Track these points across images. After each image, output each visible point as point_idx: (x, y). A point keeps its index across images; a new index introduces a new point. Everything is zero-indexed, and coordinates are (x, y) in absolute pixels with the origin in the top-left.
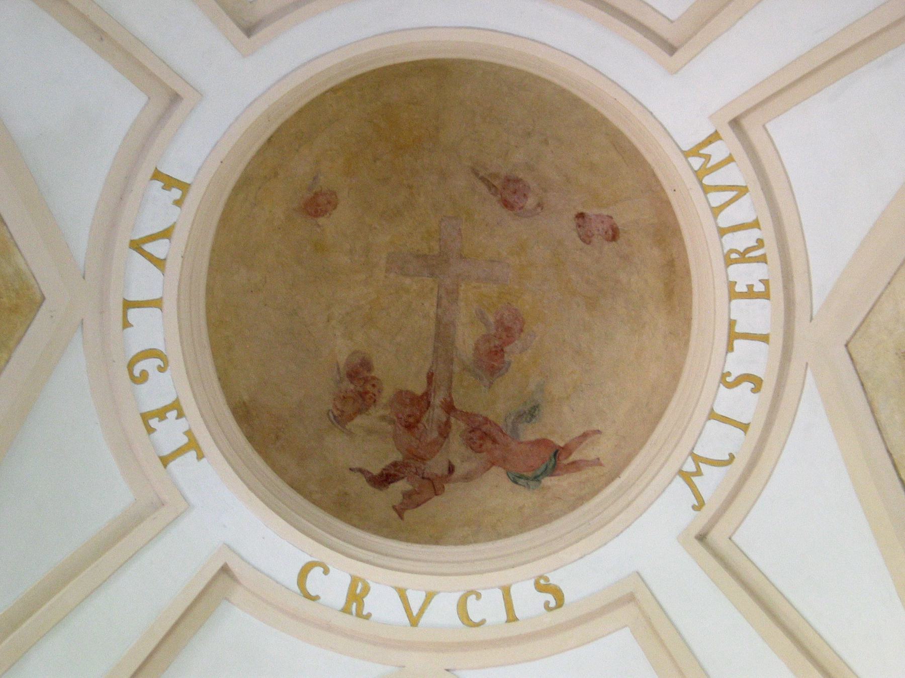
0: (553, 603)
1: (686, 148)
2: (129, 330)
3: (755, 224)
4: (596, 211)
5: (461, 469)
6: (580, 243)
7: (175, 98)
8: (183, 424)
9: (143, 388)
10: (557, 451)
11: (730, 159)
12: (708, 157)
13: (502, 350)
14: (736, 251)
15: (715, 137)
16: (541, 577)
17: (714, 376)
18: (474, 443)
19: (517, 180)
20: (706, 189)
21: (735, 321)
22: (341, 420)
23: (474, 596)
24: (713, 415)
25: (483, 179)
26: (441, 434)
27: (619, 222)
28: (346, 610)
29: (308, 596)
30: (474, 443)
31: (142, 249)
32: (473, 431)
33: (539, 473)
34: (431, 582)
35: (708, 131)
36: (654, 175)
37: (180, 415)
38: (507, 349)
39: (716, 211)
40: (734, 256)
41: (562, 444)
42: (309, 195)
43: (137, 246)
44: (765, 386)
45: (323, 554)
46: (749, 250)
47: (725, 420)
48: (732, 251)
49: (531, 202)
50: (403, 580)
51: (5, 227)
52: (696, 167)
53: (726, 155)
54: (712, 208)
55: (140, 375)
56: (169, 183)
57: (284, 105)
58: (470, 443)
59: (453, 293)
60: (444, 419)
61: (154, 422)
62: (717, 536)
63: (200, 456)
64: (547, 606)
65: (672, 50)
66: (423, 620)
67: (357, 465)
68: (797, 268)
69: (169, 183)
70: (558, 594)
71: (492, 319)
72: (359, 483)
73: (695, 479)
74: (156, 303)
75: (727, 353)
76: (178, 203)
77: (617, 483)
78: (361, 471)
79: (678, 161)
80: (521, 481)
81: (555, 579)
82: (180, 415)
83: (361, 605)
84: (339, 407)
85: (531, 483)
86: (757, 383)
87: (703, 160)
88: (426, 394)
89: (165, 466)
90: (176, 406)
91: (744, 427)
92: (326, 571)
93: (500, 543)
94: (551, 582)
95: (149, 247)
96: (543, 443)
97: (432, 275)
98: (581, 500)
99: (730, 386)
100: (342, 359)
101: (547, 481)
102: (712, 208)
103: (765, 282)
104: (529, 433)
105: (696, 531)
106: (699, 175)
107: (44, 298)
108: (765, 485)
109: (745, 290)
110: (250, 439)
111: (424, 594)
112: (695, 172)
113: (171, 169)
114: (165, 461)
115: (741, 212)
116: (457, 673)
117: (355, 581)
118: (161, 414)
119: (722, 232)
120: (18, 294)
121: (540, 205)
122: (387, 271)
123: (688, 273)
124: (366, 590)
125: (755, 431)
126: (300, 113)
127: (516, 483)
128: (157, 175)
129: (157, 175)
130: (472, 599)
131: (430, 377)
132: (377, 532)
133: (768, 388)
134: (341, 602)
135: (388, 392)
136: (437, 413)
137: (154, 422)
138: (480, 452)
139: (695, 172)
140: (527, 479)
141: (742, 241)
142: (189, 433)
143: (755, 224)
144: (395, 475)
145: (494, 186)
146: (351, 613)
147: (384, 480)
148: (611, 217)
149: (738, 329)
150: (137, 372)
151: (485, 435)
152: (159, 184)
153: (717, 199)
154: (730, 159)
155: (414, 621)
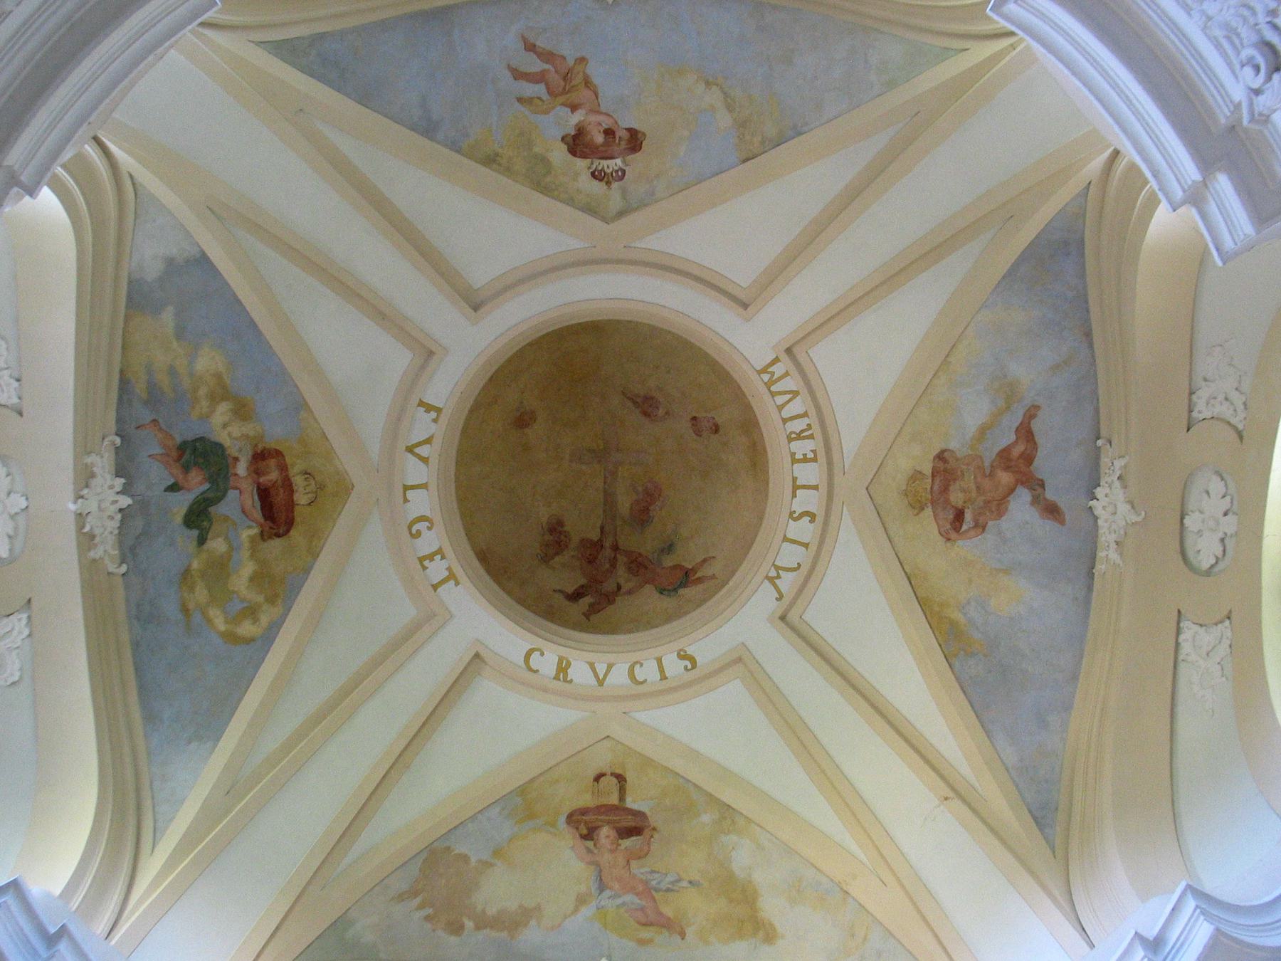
0: (689, 667)
1: (758, 368)
3: (805, 415)
4: (704, 415)
5: (626, 586)
6: (695, 437)
7: (431, 353)
8: (444, 564)
9: (418, 541)
10: (686, 573)
11: (787, 374)
12: (773, 374)
13: (648, 509)
14: (794, 433)
15: (776, 361)
16: (681, 650)
17: (785, 515)
18: (633, 570)
19: (652, 398)
20: (773, 394)
21: (797, 478)
22: (546, 559)
23: (638, 666)
24: (785, 539)
25: (629, 398)
26: (611, 566)
27: (719, 420)
28: (556, 678)
29: (531, 670)
30: (633, 570)
32: (632, 562)
33: (676, 586)
34: (611, 658)
35: (772, 357)
36: (740, 388)
37: (443, 558)
38: (652, 508)
39: (780, 408)
40: (793, 436)
41: (690, 567)
42: (519, 414)
43: (410, 450)
44: (817, 519)
45: (539, 643)
46: (802, 431)
47: (793, 542)
48: (791, 433)
49: (661, 412)
50: (591, 657)
52: (766, 381)
53: (784, 371)
54: (777, 406)
56: (429, 408)
58: (630, 570)
59: (614, 474)
60: (613, 556)
61: (426, 563)
62: (793, 616)
63: (457, 584)
64: (686, 668)
65: (745, 306)
66: (607, 681)
67: (558, 588)
68: (834, 441)
69: (429, 408)
70: (692, 660)
71: (640, 489)
72: (559, 600)
73: (777, 581)
74: (424, 486)
75: (792, 499)
76: (435, 421)
77: (727, 587)
78: (561, 591)
79: (754, 376)
80: (665, 592)
81: (690, 651)
82: (443, 558)
83: (566, 674)
84: (544, 551)
85: (673, 593)
86: (813, 517)
87: (770, 375)
88: (600, 540)
89: (435, 591)
90: (440, 551)
91: (806, 545)
92: (542, 654)
93: (654, 631)
94: (688, 653)
95: (417, 450)
96: (677, 567)
97: (599, 462)
98: (705, 601)
99: (796, 519)
100: (544, 520)
101: (682, 591)
102: (777, 406)
103: (814, 451)
104: (668, 562)
105: (779, 613)
106: (768, 385)
107: (353, 486)
109: (802, 457)
110: (488, 571)
111: (606, 665)
112: (765, 383)
113: (429, 399)
114: (435, 587)
115: (796, 407)
116: (631, 714)
117: (561, 659)
118: (431, 557)
119: (785, 421)
121: (667, 413)
122: (571, 461)
123: (765, 451)
124: (569, 664)
125: (813, 548)
126: (509, 361)
127: (662, 593)
128: (421, 404)
129: (421, 404)
130: (637, 667)
131: (602, 529)
132: (574, 629)
133: (819, 519)
134: (553, 673)
135: (575, 540)
136: (608, 552)
137: (426, 563)
138: (638, 575)
139: (765, 383)
140: (669, 590)
141: (798, 426)
142: (449, 569)
143: (805, 415)
144: (584, 593)
145: (637, 402)
146: (560, 680)
147: (575, 596)
148: (714, 418)
149: (798, 483)
151: (640, 565)
152: (422, 409)
153: (780, 400)
154: (787, 374)
155: (601, 683)
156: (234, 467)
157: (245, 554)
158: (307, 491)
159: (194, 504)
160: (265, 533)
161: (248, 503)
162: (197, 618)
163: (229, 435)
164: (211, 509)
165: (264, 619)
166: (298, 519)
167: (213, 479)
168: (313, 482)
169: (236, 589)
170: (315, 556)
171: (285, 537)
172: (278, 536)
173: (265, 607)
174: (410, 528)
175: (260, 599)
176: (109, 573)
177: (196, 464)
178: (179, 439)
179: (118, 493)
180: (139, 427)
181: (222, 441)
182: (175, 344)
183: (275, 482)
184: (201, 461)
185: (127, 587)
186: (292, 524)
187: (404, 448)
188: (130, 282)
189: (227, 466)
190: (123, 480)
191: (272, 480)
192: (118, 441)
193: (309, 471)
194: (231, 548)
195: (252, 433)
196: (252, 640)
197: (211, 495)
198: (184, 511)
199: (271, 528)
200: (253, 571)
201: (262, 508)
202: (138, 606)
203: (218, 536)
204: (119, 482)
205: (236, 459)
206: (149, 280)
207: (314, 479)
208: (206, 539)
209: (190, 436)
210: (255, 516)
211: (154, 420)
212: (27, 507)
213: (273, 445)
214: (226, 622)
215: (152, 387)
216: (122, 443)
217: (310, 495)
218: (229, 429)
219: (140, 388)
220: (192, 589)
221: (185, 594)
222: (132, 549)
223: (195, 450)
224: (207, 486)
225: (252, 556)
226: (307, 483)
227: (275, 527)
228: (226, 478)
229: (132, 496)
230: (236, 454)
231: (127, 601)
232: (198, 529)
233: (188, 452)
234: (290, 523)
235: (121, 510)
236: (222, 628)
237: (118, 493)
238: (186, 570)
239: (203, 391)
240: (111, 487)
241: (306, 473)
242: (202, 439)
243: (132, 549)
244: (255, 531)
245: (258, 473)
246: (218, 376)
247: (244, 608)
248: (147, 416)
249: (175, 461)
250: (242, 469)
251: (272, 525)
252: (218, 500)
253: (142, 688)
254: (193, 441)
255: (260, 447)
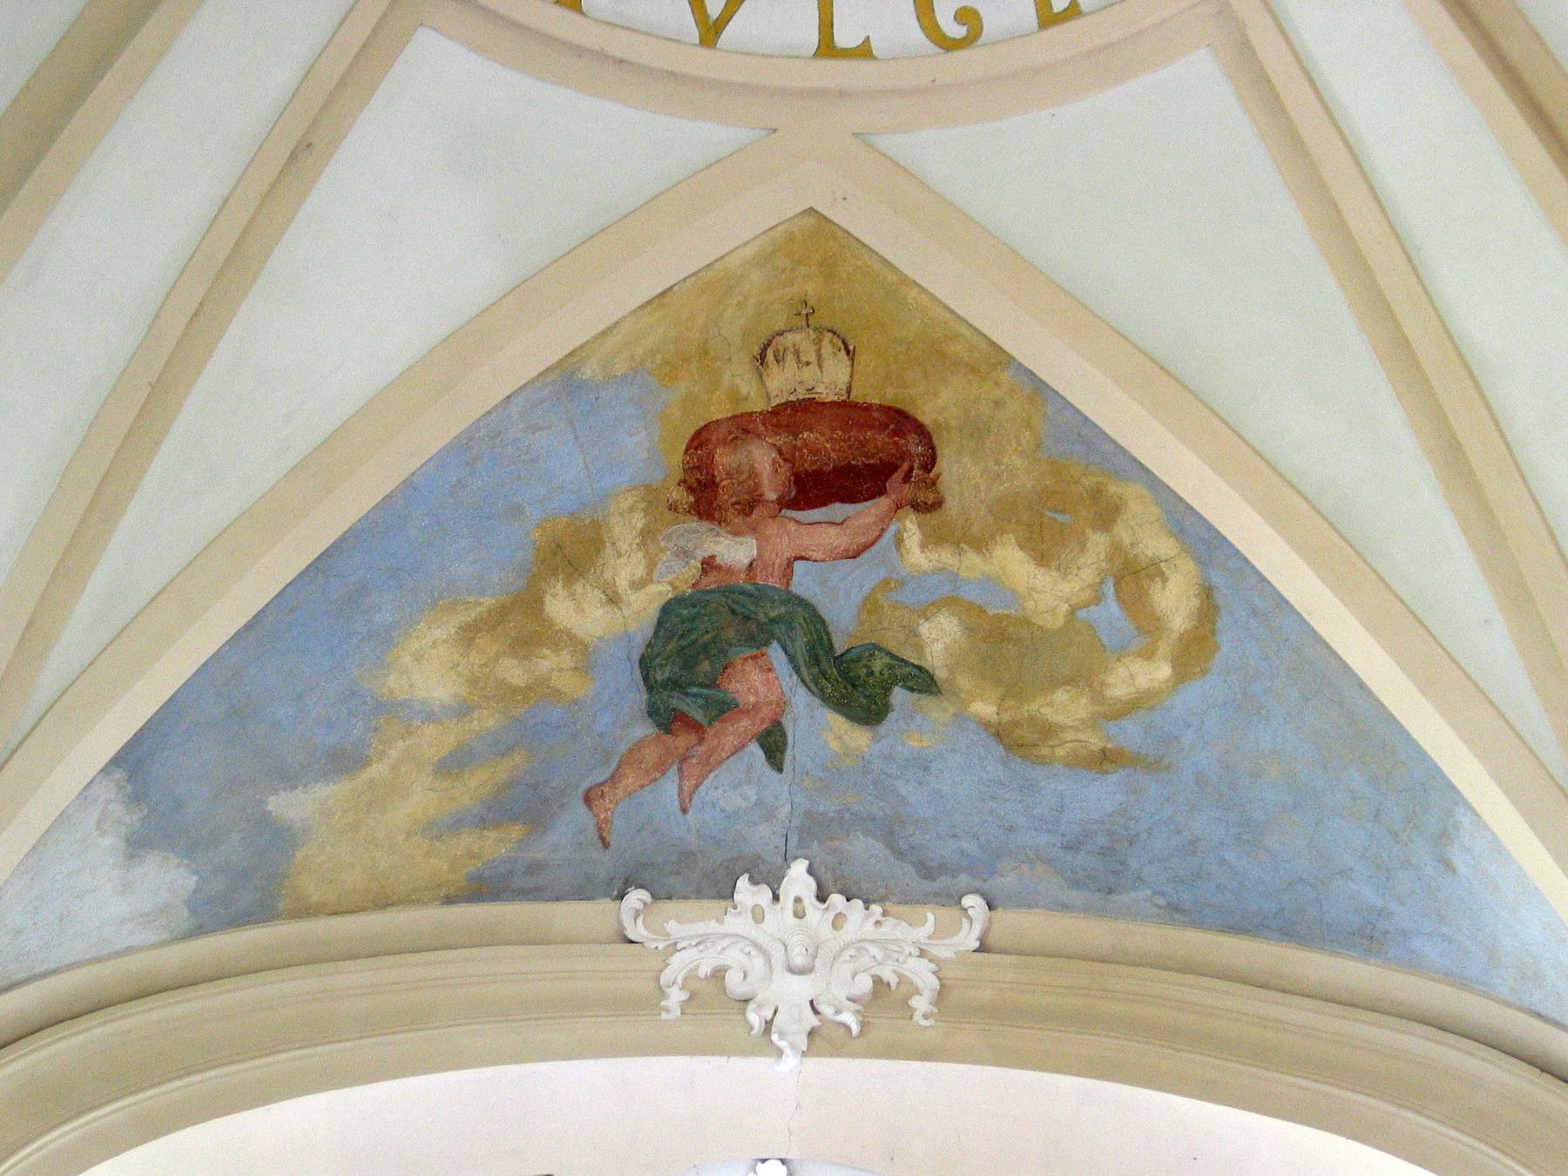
2: (875, 45)
9: (993, 22)
31: (717, 19)
51: (675, 288)
55: (965, 24)
57: (699, 290)
108: (1559, 550)
120: (799, 262)
150: (957, 31)
156: (729, 571)
157: (971, 564)
158: (812, 357)
159: (826, 700)
160: (921, 497)
161: (833, 538)
162: (1129, 734)
163: (638, 585)
164: (840, 645)
165: (1157, 544)
166: (889, 395)
167: (758, 636)
168: (790, 338)
169: (1065, 607)
170: (1000, 358)
171: (936, 442)
172: (930, 462)
173: (1122, 532)
174: (948, 45)
175: (1098, 542)
176: (983, 948)
177: (712, 684)
178: (644, 729)
179: (776, 898)
180: (602, 839)
181: (653, 612)
182: (376, 770)
183: (780, 452)
184: (705, 666)
185: (1025, 902)
186: (901, 414)
187: (705, 53)
188: (199, 931)
189: (728, 591)
190: (743, 883)
191: (774, 462)
192: (636, 897)
193: (756, 350)
194: (950, 603)
195: (639, 521)
196: (1207, 592)
197: (800, 645)
198: (836, 722)
199: (907, 478)
200: (1021, 547)
201: (850, 498)
202: (1075, 884)
203: (914, 633)
204: (747, 892)
205: (709, 565)
206: (192, 881)
207: (780, 334)
208: (919, 668)
209: (638, 697)
210: (871, 520)
211: (588, 799)
212: (783, 1161)
213: (676, 458)
214: (1148, 654)
215: (494, 813)
216: (642, 887)
217: (827, 349)
218: (622, 584)
219: (495, 845)
220: (1048, 731)
221: (1060, 752)
222: (927, 871)
223: (674, 684)
224: (775, 653)
225: (980, 545)
226: (790, 357)
227: (905, 466)
228: (759, 595)
229: (787, 860)
230: (696, 564)
231: (1065, 907)
232: (890, 689)
233: (678, 702)
234: (900, 421)
235: (822, 897)
236: (1164, 671)
237: (776, 898)
238: (998, 735)
239: (514, 672)
240: (758, 915)
241: (762, 357)
242: (646, 664)
243: (927, 871)
244: (911, 527)
245: (750, 504)
246: (468, 635)
247: (1119, 599)
248: (575, 819)
249: (701, 740)
250: (736, 551)
251: (898, 476)
252: (816, 621)
253: (1289, 930)
254: (650, 689)
255: (680, 495)
